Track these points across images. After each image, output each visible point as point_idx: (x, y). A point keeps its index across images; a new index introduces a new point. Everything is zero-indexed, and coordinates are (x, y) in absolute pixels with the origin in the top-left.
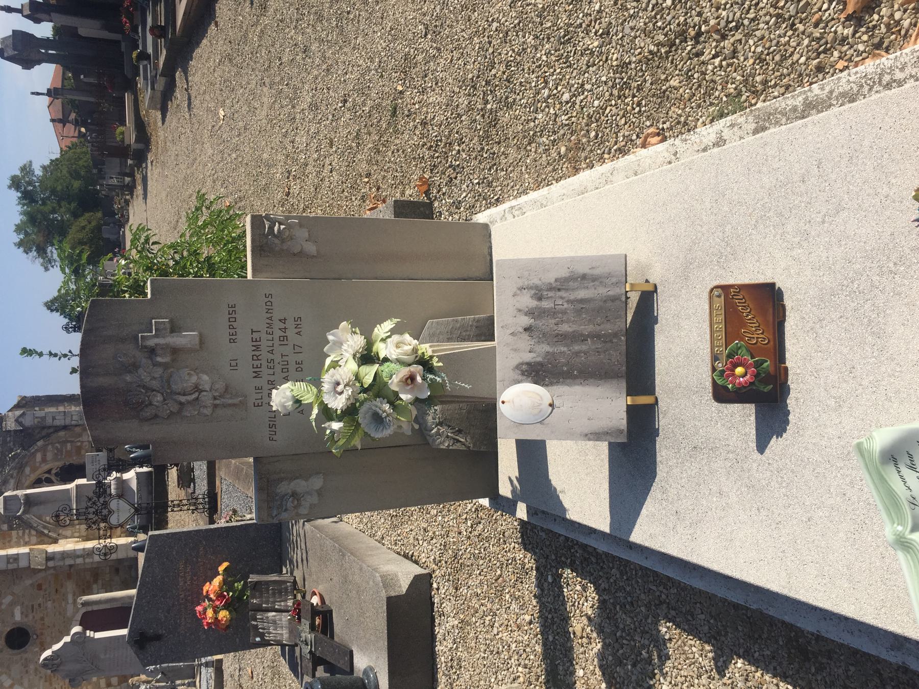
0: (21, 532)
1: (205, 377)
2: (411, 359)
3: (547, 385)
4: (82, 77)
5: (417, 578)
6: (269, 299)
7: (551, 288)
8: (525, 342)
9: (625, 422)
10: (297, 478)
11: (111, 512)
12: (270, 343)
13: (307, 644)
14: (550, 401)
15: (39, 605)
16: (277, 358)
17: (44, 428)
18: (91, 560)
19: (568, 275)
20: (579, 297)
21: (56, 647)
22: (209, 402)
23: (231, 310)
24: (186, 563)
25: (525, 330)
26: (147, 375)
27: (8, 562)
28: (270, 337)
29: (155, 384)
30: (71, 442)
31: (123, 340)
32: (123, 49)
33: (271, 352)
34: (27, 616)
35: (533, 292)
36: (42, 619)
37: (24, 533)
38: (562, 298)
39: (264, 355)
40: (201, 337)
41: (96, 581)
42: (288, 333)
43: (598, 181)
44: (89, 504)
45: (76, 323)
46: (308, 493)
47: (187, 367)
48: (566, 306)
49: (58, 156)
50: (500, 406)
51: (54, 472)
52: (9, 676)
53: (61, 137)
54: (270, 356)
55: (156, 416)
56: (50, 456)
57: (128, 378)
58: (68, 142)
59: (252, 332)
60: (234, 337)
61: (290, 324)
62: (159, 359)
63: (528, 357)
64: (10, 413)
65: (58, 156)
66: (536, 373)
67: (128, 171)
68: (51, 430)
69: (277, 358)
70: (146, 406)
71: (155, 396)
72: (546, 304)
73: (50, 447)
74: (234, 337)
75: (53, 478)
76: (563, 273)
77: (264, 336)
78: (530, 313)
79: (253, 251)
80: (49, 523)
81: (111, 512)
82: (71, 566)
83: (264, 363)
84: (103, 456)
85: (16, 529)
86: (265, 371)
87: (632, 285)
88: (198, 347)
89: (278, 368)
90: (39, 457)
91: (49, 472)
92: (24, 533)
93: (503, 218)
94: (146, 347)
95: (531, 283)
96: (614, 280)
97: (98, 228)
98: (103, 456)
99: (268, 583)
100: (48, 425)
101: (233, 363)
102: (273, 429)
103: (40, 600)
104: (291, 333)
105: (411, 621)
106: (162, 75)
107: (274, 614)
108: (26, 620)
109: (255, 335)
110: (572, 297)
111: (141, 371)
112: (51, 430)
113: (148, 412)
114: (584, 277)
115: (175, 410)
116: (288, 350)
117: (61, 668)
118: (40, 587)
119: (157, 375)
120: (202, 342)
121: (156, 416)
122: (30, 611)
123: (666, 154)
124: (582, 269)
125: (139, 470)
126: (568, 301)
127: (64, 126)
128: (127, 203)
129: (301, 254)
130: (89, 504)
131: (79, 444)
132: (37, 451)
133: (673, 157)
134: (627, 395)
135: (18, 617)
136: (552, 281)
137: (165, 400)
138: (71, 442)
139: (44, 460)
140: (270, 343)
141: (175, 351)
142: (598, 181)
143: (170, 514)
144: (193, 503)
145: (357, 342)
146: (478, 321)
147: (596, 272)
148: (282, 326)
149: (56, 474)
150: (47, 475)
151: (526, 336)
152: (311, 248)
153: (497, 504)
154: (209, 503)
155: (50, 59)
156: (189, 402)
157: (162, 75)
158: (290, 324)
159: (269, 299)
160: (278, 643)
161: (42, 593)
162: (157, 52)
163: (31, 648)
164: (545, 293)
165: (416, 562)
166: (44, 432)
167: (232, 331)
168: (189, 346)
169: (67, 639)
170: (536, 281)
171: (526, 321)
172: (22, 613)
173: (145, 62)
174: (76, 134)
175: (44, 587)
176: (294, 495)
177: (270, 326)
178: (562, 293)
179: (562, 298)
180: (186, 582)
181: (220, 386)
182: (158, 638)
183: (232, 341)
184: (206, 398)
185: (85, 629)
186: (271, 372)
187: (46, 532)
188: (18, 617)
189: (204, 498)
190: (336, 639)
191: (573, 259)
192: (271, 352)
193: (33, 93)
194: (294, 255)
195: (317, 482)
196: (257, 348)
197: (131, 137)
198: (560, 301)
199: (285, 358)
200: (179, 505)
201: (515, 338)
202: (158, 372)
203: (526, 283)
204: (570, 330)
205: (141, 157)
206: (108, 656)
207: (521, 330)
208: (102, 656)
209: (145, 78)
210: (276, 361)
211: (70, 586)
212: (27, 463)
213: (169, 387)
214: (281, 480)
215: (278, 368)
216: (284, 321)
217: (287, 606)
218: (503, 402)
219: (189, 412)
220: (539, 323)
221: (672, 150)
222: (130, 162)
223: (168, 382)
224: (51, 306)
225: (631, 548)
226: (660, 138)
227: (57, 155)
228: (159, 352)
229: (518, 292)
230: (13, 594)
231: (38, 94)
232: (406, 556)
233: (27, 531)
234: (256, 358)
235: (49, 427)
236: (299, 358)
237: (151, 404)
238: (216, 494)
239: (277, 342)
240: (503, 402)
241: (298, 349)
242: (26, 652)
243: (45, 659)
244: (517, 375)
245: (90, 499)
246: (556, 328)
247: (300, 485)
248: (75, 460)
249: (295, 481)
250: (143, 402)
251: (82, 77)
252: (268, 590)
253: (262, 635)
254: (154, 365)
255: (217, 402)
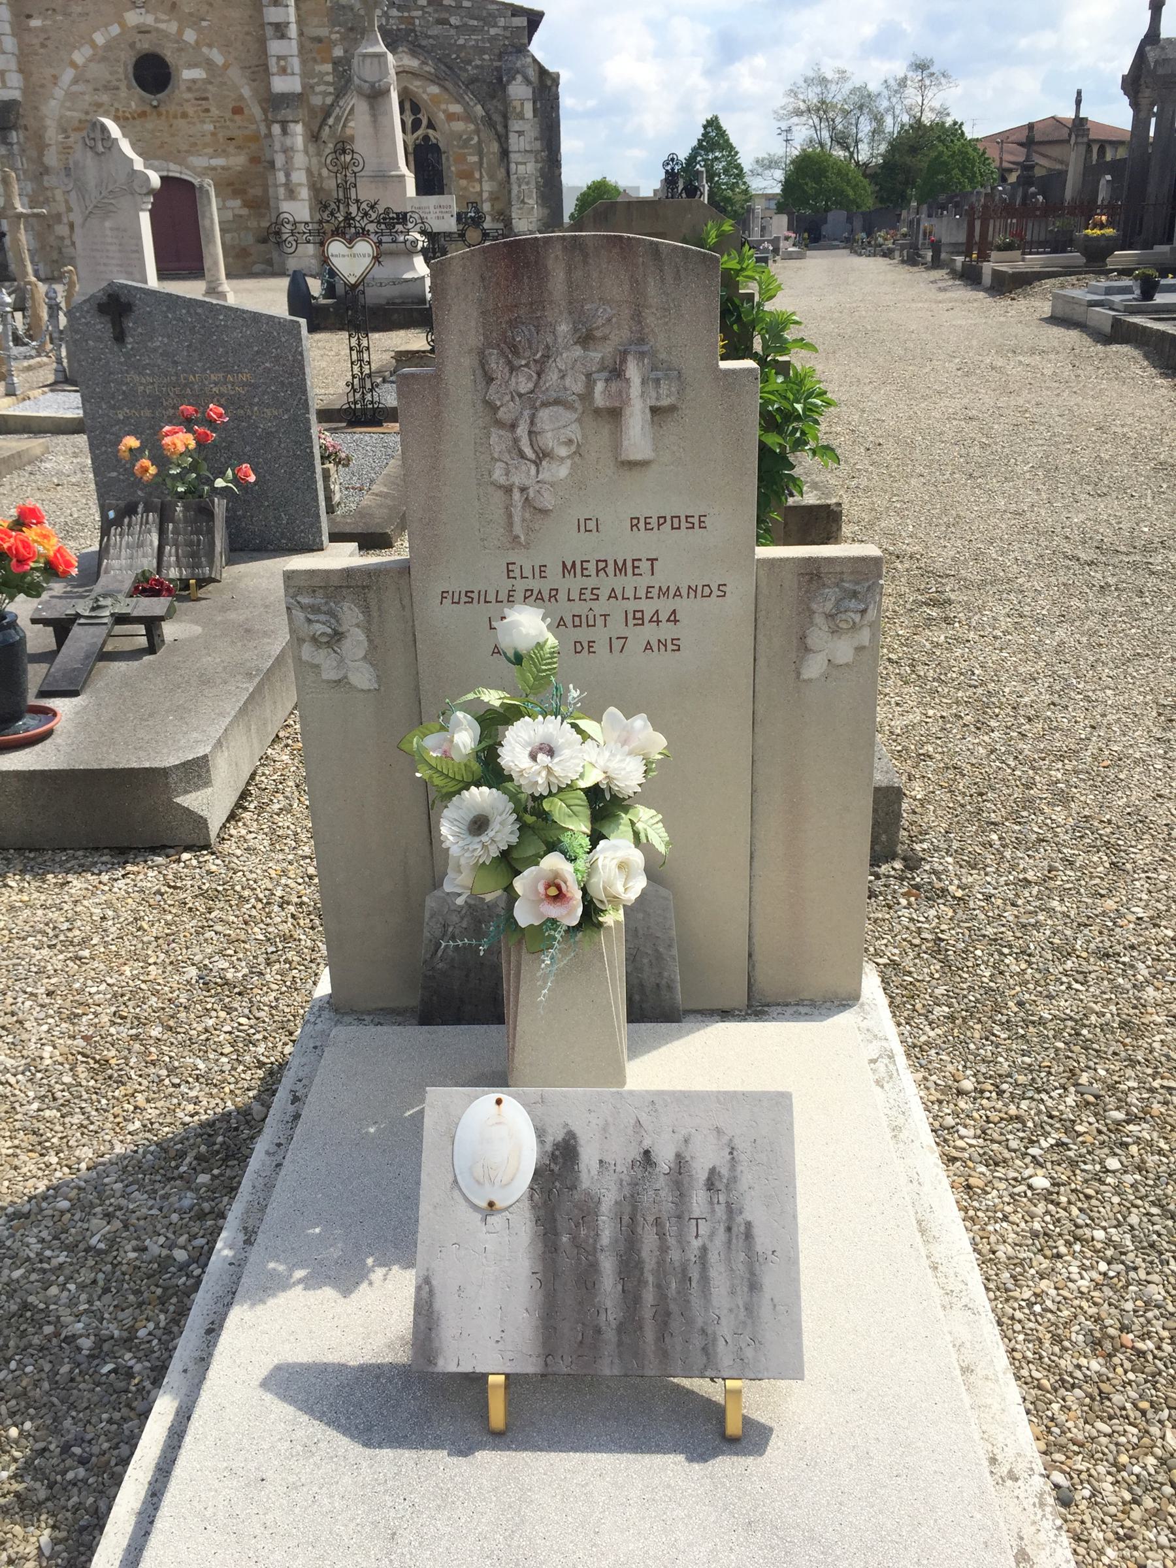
0: (330, 78)
1: (563, 471)
2: (597, 893)
3: (531, 1198)
4: (1109, 177)
5: (201, 823)
6: (716, 592)
7: (731, 1211)
8: (622, 1153)
9: (452, 1368)
10: (370, 641)
11: (350, 242)
12: (629, 593)
13: (93, 609)
14: (499, 1204)
15: (207, 110)
16: (600, 607)
17: (505, 117)
18: (281, 197)
19: (759, 1248)
20: (713, 1273)
21: (125, 146)
22: (517, 479)
23: (696, 520)
24: (251, 385)
25: (647, 1153)
26: (570, 366)
27: (279, 58)
28: (642, 593)
29: (552, 377)
30: (481, 163)
31: (637, 317)
32: (1159, 248)
33: (613, 595)
34: (189, 89)
35: (725, 1171)
36: (184, 115)
37: (328, 84)
38: (712, 1234)
39: (607, 583)
40: (643, 464)
41: (246, 204)
42: (649, 628)
43: (951, 1272)
44: (364, 206)
45: (681, 179)
46: (342, 660)
47: (584, 436)
48: (696, 1243)
49: (969, 136)
50: (493, 1094)
51: (430, 132)
52: (90, 60)
53: (1001, 139)
54: (604, 593)
55: (490, 380)
56: (458, 126)
57: (563, 328)
58: (993, 153)
59: (652, 560)
60: (642, 525)
61: (667, 631)
62: (600, 386)
63: (588, 1157)
64: (529, 60)
65: (969, 136)
66: (559, 1162)
67: (943, 256)
68: (500, 128)
69: (600, 607)
70: (509, 362)
71: (530, 378)
72: (698, 1200)
73: (472, 127)
74: (642, 525)
75: (420, 132)
76: (763, 1241)
77: (643, 582)
78: (681, 1163)
79: (809, 561)
80: (344, 126)
81: (350, 242)
82: (272, 164)
83: (590, 583)
84: (450, 224)
85: (334, 70)
86: (575, 583)
87: (738, 1392)
88: (623, 457)
89: (580, 608)
90: (456, 108)
91: (431, 125)
92: (328, 84)
93: (873, 1036)
94: (623, 361)
95: (742, 1167)
96: (749, 1353)
97: (843, 201)
98: (450, 224)
99: (211, 532)
100: (510, 122)
101: (591, 525)
102: (464, 599)
103: (215, 112)
104: (649, 632)
105: (119, 820)
106: (1116, 322)
107: (156, 543)
108: (183, 88)
109: (645, 566)
110: (713, 1257)
111: (578, 351)
112: (500, 128)
113: (496, 365)
114: (754, 1286)
115: (501, 414)
116: (617, 627)
117: (90, 154)
118: (238, 111)
119: (568, 381)
120: (632, 465)
121: (490, 380)
122: (197, 95)
123: (1010, 1452)
124: (770, 1280)
125: (428, 282)
126: (704, 1249)
127: (1021, 144)
128: (887, 254)
129: (804, 648)
130: (364, 206)
131: (477, 175)
132: (466, 106)
133: (1004, 1471)
134: (507, 1376)
135: (188, 74)
136: (748, 1215)
137: (520, 395)
138: (481, 163)
139: (451, 117)
140: (629, 593)
141: (614, 414)
142: (951, 1272)
143: (345, 335)
144: (364, 382)
145: (629, 776)
146: (670, 988)
147: (765, 1311)
148: (663, 617)
149: (426, 138)
150: (425, 122)
151: (635, 1153)
152: (814, 668)
153: (321, 1009)
154: (364, 410)
155: (1140, 123)
156: (516, 441)
157: (1116, 322)
158: (667, 631)
159: (716, 592)
160: (103, 552)
161: (228, 115)
162: (1156, 312)
163: (133, 98)
164: (722, 1198)
165: (232, 817)
166: (497, 118)
167: (654, 522)
168: (625, 443)
169: (139, 164)
170: (747, 1177)
171: (665, 1157)
172: (194, 81)
173: (1138, 292)
174: (1006, 165)
175: (237, 117)
176: (337, 636)
177: (664, 593)
178: (721, 1235)
179: (712, 1234)
180: (216, 384)
181: (548, 500)
182: (120, 337)
183: (634, 523)
184: (524, 475)
185: (156, 194)
186: (575, 595)
187: (331, 121)
188: (188, 74)
189: (372, 402)
190: (101, 664)
191: (793, 1262)
192: (613, 595)
193: (1079, 93)
194: (803, 638)
195: (362, 677)
196: (620, 569)
197: (997, 263)
198: (704, 1233)
199: (600, 621)
200: (360, 352)
201: (630, 1131)
202: (576, 385)
203: (743, 1157)
204: (645, 1254)
205: (970, 277)
206: (108, 233)
207: (646, 1144)
208: (107, 224)
209: (1109, 291)
210: (593, 604)
211: (237, 161)
212: (446, 89)
213: (545, 405)
214: (366, 610)
215: (580, 608)
216: (673, 618)
217: (169, 567)
218: (499, 1102)
219: (498, 440)
220: (661, 1182)
221: (1020, 1468)
222: (960, 259)
223: (557, 402)
224: (714, 137)
225: (209, 1331)
226: (1044, 1472)
227: (970, 133)
228: (614, 386)
229: (725, 1139)
230: (226, 66)
231: (1078, 102)
232: (244, 795)
233: (331, 89)
234: (602, 567)
235: (506, 127)
236: (601, 647)
237: (513, 369)
238: (379, 424)
239: (632, 606)
240: (499, 1102)
241: (617, 645)
242: (129, 88)
243: (104, 128)
244: (556, 1134)
245: (372, 207)
246: (651, 1219)
247: (356, 642)
248: (451, 168)
249: (362, 637)
250: (516, 353)
251: (1109, 177)
252: (198, 532)
253: (118, 522)
254: (588, 376)
255: (517, 495)
